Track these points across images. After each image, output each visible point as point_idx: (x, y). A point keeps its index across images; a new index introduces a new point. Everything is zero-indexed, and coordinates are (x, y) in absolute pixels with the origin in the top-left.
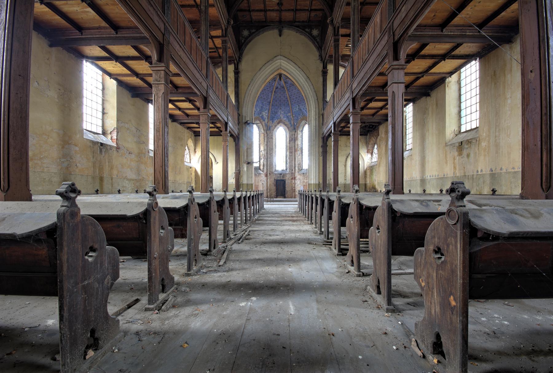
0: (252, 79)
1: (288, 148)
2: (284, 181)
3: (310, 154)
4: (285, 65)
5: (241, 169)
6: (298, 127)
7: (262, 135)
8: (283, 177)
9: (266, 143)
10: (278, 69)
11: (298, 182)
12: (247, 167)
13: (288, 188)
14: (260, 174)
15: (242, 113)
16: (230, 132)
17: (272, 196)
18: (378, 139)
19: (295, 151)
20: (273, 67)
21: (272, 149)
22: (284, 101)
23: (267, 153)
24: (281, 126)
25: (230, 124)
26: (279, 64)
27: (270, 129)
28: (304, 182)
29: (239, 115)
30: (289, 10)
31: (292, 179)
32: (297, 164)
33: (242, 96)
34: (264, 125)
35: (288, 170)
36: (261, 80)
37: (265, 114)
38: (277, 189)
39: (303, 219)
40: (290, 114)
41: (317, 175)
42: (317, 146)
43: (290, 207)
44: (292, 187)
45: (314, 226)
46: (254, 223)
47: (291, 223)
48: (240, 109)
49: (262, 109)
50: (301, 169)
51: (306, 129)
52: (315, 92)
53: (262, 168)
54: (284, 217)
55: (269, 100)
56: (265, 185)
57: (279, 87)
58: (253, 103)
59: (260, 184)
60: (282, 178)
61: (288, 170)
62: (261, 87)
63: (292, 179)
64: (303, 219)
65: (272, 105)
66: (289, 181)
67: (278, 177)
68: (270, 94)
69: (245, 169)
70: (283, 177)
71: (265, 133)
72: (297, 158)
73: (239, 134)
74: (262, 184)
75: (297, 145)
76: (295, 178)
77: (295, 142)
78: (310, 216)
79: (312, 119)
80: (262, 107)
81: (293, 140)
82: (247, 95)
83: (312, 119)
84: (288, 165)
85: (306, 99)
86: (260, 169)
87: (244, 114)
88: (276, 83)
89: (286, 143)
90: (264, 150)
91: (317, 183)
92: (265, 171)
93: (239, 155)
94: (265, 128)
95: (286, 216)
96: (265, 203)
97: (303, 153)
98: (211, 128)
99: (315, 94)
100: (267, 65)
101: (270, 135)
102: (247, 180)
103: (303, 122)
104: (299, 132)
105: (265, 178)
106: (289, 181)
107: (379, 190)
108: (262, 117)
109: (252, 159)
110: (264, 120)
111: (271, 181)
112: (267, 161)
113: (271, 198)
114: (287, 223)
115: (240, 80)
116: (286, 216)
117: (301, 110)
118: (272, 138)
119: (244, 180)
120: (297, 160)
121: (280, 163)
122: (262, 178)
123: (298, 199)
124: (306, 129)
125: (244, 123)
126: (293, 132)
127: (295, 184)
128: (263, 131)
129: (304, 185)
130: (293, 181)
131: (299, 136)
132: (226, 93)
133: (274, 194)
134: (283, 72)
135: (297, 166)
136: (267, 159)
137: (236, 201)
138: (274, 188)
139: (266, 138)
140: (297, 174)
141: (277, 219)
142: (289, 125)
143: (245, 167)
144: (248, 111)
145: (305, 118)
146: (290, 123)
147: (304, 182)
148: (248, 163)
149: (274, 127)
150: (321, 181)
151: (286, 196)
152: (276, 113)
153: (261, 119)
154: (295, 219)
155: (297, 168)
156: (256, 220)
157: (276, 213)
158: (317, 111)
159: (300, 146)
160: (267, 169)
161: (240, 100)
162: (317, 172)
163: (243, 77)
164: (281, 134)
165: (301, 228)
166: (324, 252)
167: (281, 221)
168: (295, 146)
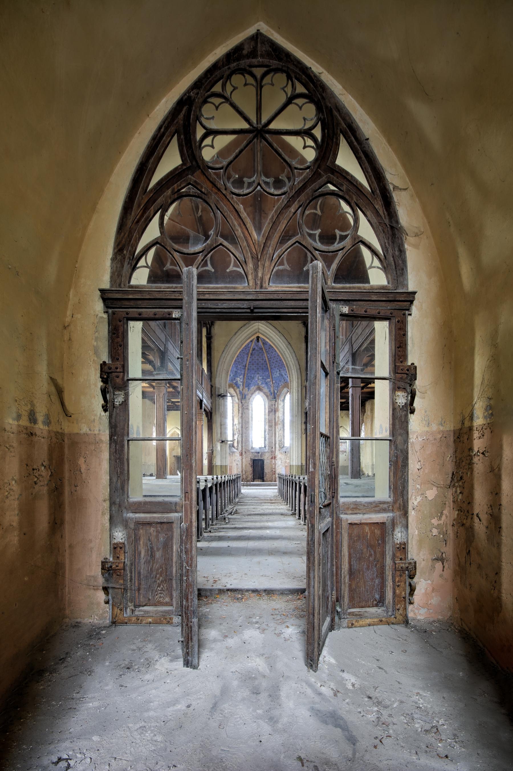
0: (227, 345)
1: (267, 421)
2: (262, 461)
3: (292, 432)
4: (263, 329)
5: (214, 449)
6: (279, 396)
7: (237, 405)
8: (261, 456)
9: (240, 415)
10: (256, 333)
11: (278, 462)
12: (221, 446)
13: (267, 470)
14: (234, 452)
15: (215, 384)
16: (205, 410)
17: (249, 479)
18: (365, 417)
19: (275, 425)
20: (250, 331)
21: (248, 422)
22: (262, 364)
23: (242, 427)
24: (259, 393)
25: (205, 401)
26: (256, 327)
27: (245, 398)
28: (286, 462)
29: (212, 386)
30: (270, 514)
31: (272, 458)
32: (277, 440)
33: (215, 364)
34: (238, 392)
35: (267, 448)
36: (236, 345)
37: (239, 380)
38: (254, 471)
39: (281, 501)
40: (269, 380)
41: (300, 455)
42: (300, 422)
43: (270, 491)
44: (272, 468)
45: (302, 523)
46: (237, 504)
47: (269, 504)
48: (213, 379)
49: (236, 374)
50: (282, 447)
51: (288, 397)
52: (297, 360)
53: (236, 445)
54: (263, 500)
55: (244, 364)
56: (240, 466)
57: (256, 348)
58: (228, 372)
59: (234, 464)
60: (260, 458)
61: (267, 448)
62: (236, 354)
63: (272, 458)
64: (281, 501)
65: (248, 369)
66: (268, 461)
67: (255, 456)
68: (246, 356)
69: (219, 448)
70: (261, 456)
71: (240, 403)
72: (277, 434)
73: (211, 409)
74: (236, 465)
75: (278, 417)
76: (275, 458)
77: (275, 414)
78: (294, 505)
79: (294, 391)
80: (236, 372)
81: (273, 410)
82: (220, 363)
83: (294, 391)
84: (267, 442)
85: (288, 367)
86: (233, 446)
87: (217, 385)
88: (253, 344)
89: (265, 415)
90: (239, 423)
91: (300, 464)
92: (240, 449)
93: (212, 432)
94: (240, 397)
95: (265, 500)
96: (242, 487)
97: (285, 427)
98: (178, 402)
99: (297, 363)
100: (243, 329)
101: (246, 405)
102: (221, 461)
103: (285, 390)
104: (280, 402)
105: (240, 457)
106: (268, 461)
107: (366, 473)
108: (236, 384)
109: (226, 438)
110: (238, 387)
111: (247, 461)
112: (242, 437)
113: (248, 482)
114: (266, 504)
115: (212, 346)
116: (265, 500)
117: (282, 375)
118: (248, 409)
119: (218, 462)
120: (277, 435)
121: (258, 440)
122: (236, 458)
123: (277, 483)
124: (288, 397)
125: (217, 396)
126: (273, 402)
127: (275, 464)
128: (237, 400)
129: (286, 466)
130: (273, 461)
131: (280, 407)
132: (201, 369)
133: (250, 477)
134: (260, 336)
135: (277, 442)
136: (242, 434)
137: (218, 486)
138: (250, 469)
139: (240, 409)
140: (277, 453)
141: (256, 502)
142: (269, 394)
143: (218, 446)
144: (222, 381)
145: (286, 385)
146: (270, 391)
147: (286, 462)
148: (222, 442)
149: (250, 395)
150: (304, 463)
151: (265, 479)
152: (253, 378)
153: (234, 385)
154: (273, 501)
155: (277, 446)
156: (238, 502)
157: (255, 497)
158: (300, 382)
159: (281, 418)
160: (242, 447)
161: (213, 369)
162: (300, 452)
163: (217, 343)
164: (258, 403)
165: (278, 507)
166: (292, 518)
167: (261, 503)
168: (275, 419)
